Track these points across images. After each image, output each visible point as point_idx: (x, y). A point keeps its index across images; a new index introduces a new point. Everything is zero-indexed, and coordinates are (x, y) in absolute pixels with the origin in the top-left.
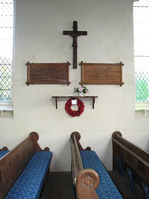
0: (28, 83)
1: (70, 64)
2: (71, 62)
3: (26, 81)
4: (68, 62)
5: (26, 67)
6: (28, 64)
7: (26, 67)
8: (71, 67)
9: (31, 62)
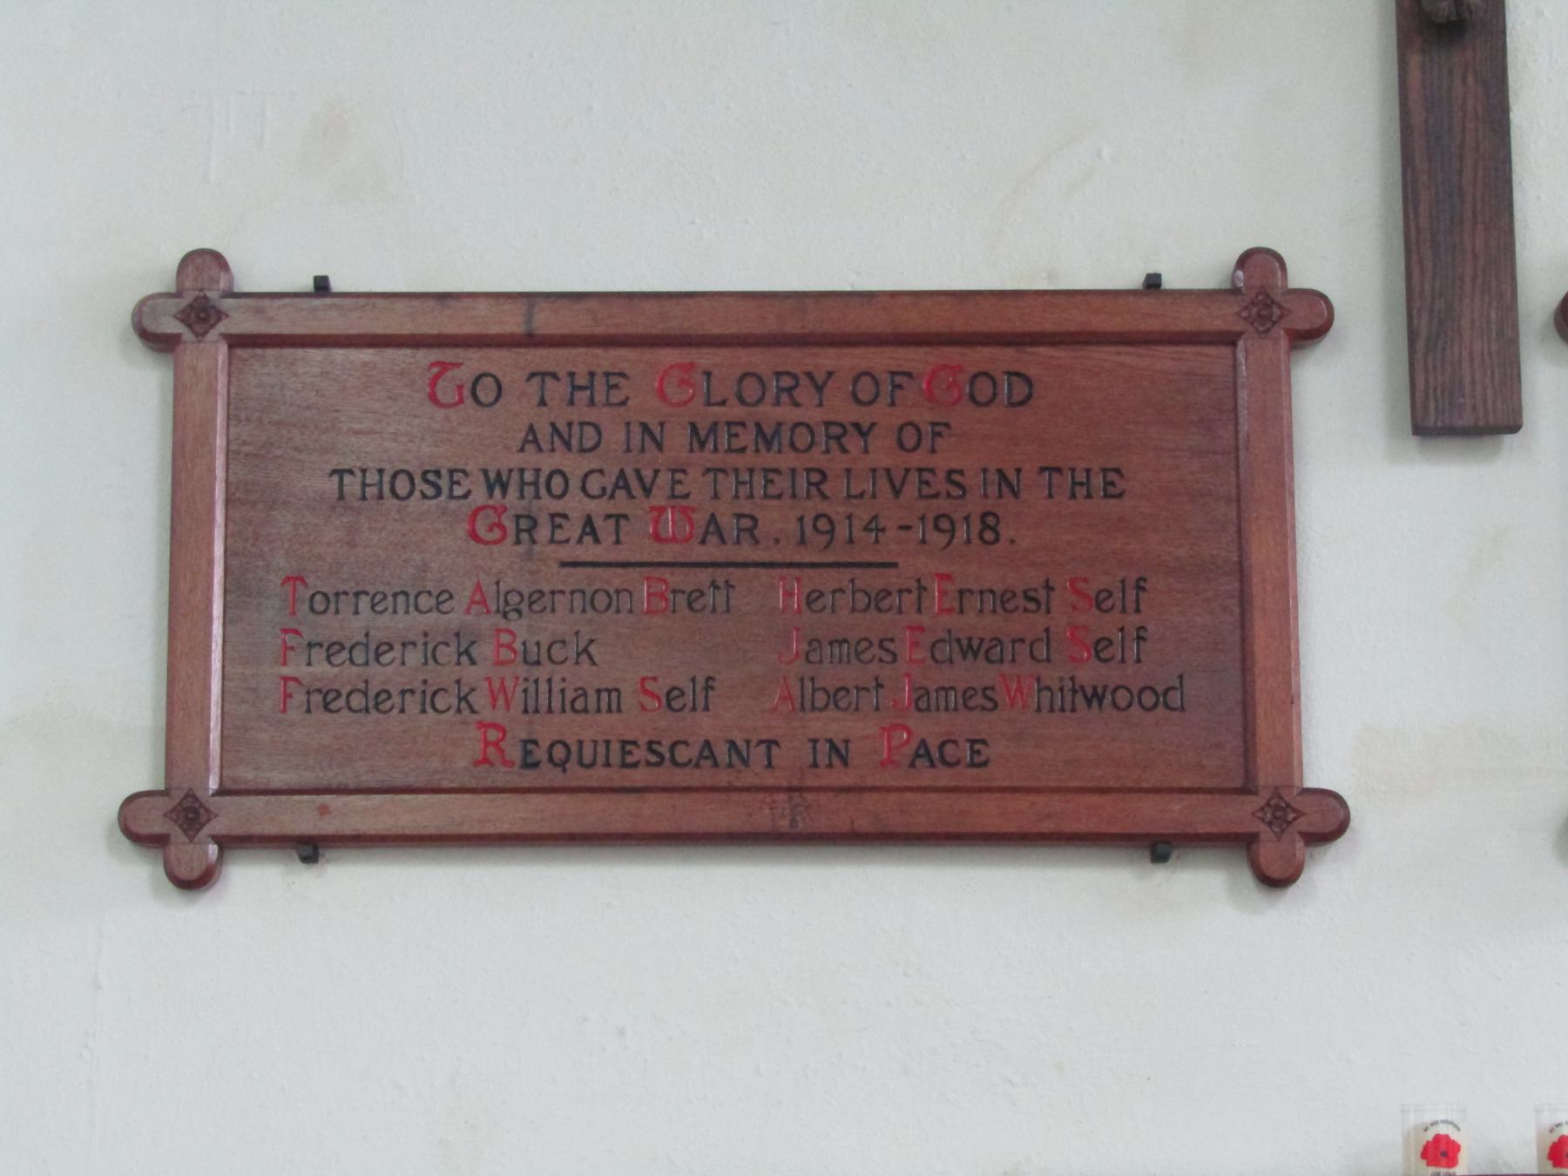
0: (180, 833)
1: (1309, 322)
2: (1342, 246)
3: (140, 771)
4: (1259, 264)
5: (124, 417)
6: (193, 316)
7: (145, 386)
8: (1339, 401)
9: (268, 263)
